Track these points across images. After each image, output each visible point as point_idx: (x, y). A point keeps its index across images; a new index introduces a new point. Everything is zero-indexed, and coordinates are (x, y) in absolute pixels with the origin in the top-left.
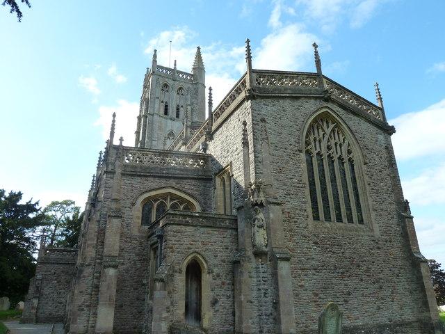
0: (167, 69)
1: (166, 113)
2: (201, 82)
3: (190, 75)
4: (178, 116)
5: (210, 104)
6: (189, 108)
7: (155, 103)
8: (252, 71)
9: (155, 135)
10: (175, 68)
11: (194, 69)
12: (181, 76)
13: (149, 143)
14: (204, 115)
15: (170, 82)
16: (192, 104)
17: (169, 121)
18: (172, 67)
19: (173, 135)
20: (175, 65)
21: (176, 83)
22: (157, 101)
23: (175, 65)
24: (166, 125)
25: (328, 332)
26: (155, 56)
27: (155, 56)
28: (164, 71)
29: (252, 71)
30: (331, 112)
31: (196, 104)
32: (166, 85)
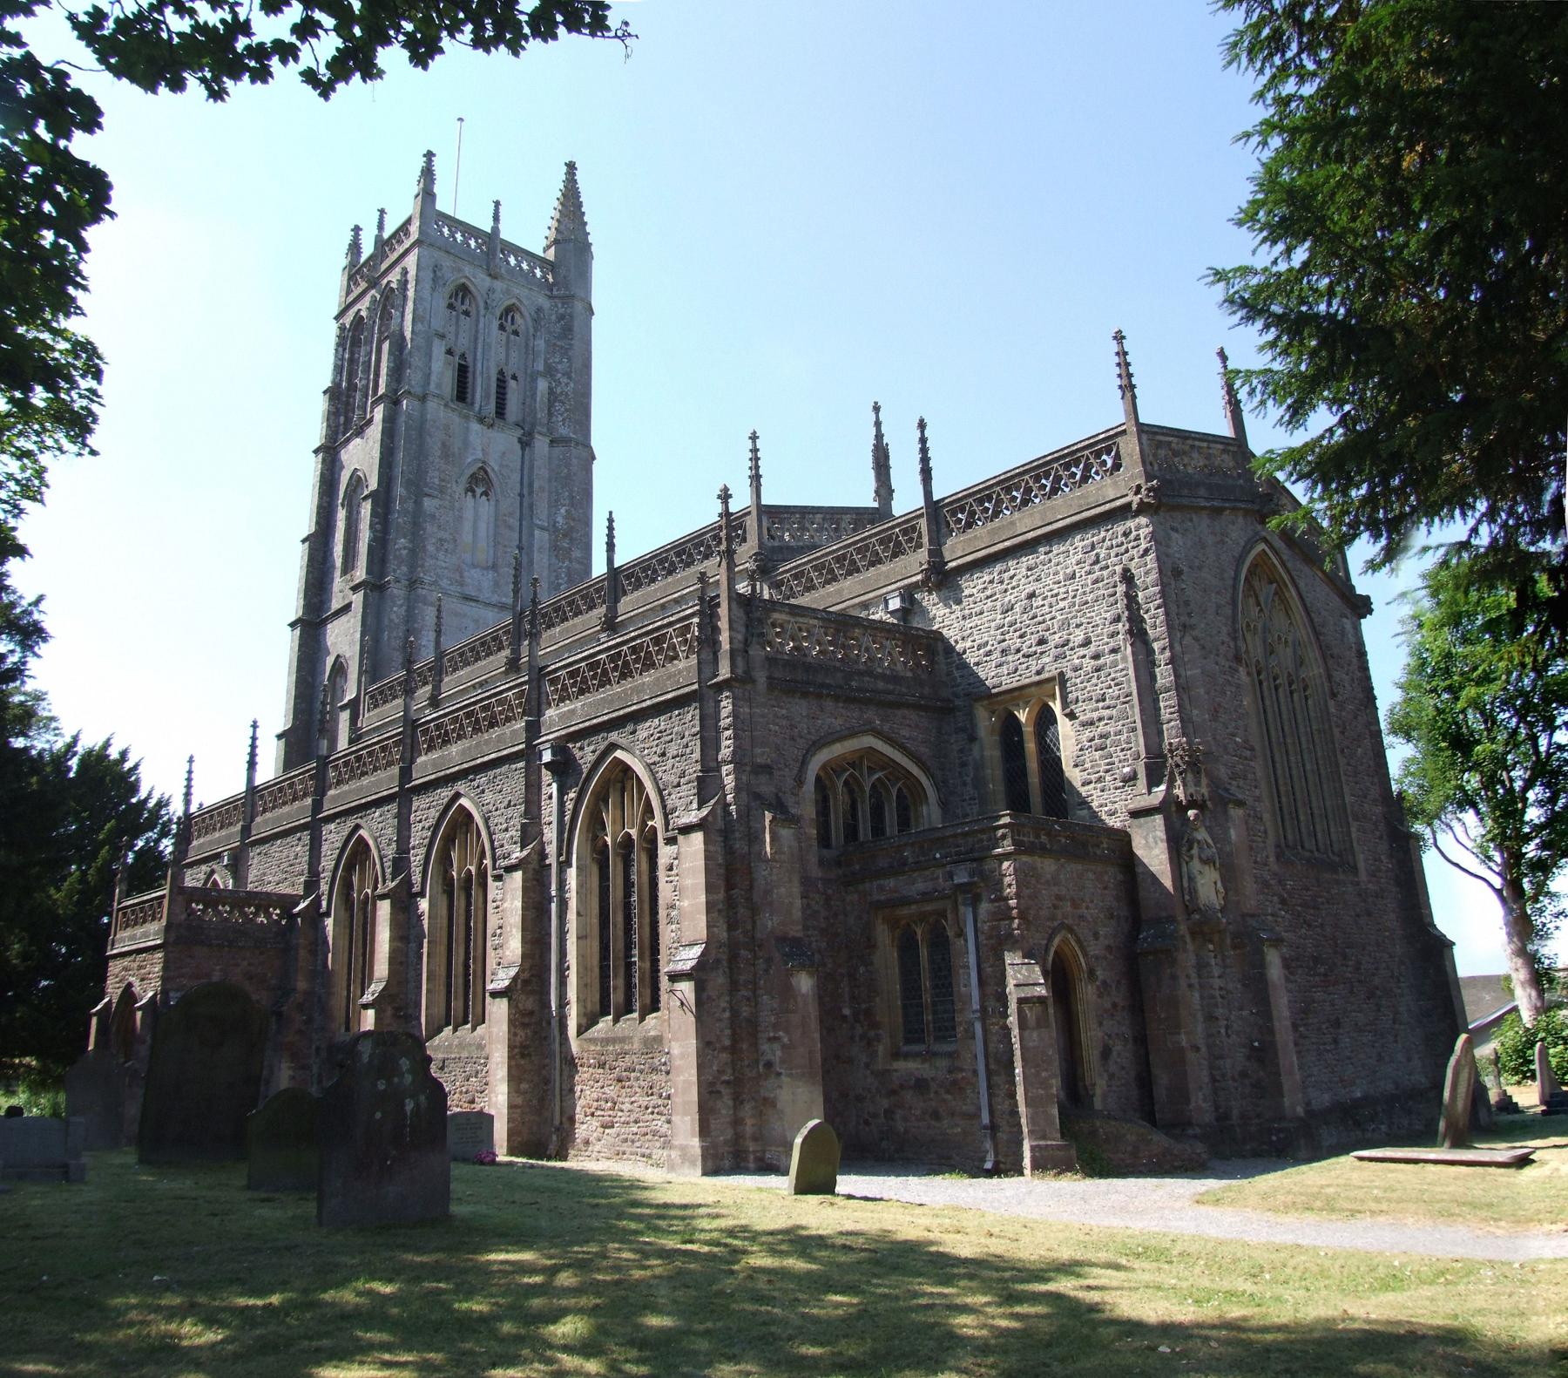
0: (470, 231)
1: (462, 392)
2: (582, 295)
3: (543, 262)
4: (501, 411)
5: (611, 547)
6: (542, 385)
7: (429, 355)
8: (759, 505)
9: (433, 477)
10: (496, 230)
11: (556, 242)
12: (512, 261)
13: (410, 506)
14: (550, 1007)
15: (480, 281)
16: (550, 371)
17: (475, 427)
18: (487, 226)
19: (488, 482)
20: (496, 218)
21: (498, 285)
22: (439, 349)
23: (496, 218)
24: (466, 443)
25: (1564, 1329)
26: (428, 174)
27: (428, 174)
28: (459, 237)
29: (759, 505)
30: (1271, 555)
31: (568, 375)
32: (463, 291)
